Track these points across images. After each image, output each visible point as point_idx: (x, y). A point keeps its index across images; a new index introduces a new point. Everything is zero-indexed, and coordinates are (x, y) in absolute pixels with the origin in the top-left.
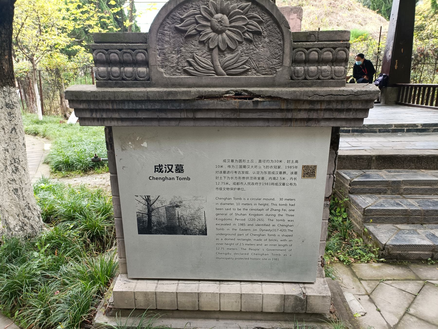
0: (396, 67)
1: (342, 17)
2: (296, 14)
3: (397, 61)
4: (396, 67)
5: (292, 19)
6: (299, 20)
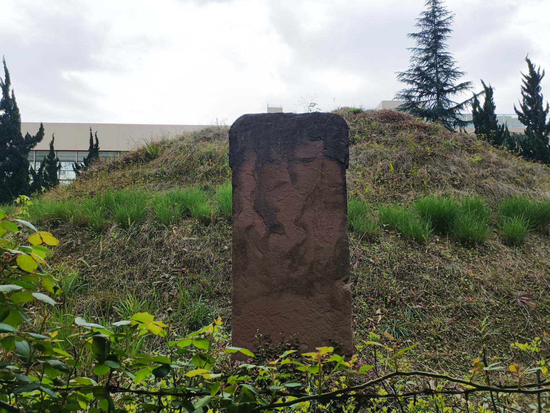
1: (460, 164)
5: (304, 160)
6: (332, 167)
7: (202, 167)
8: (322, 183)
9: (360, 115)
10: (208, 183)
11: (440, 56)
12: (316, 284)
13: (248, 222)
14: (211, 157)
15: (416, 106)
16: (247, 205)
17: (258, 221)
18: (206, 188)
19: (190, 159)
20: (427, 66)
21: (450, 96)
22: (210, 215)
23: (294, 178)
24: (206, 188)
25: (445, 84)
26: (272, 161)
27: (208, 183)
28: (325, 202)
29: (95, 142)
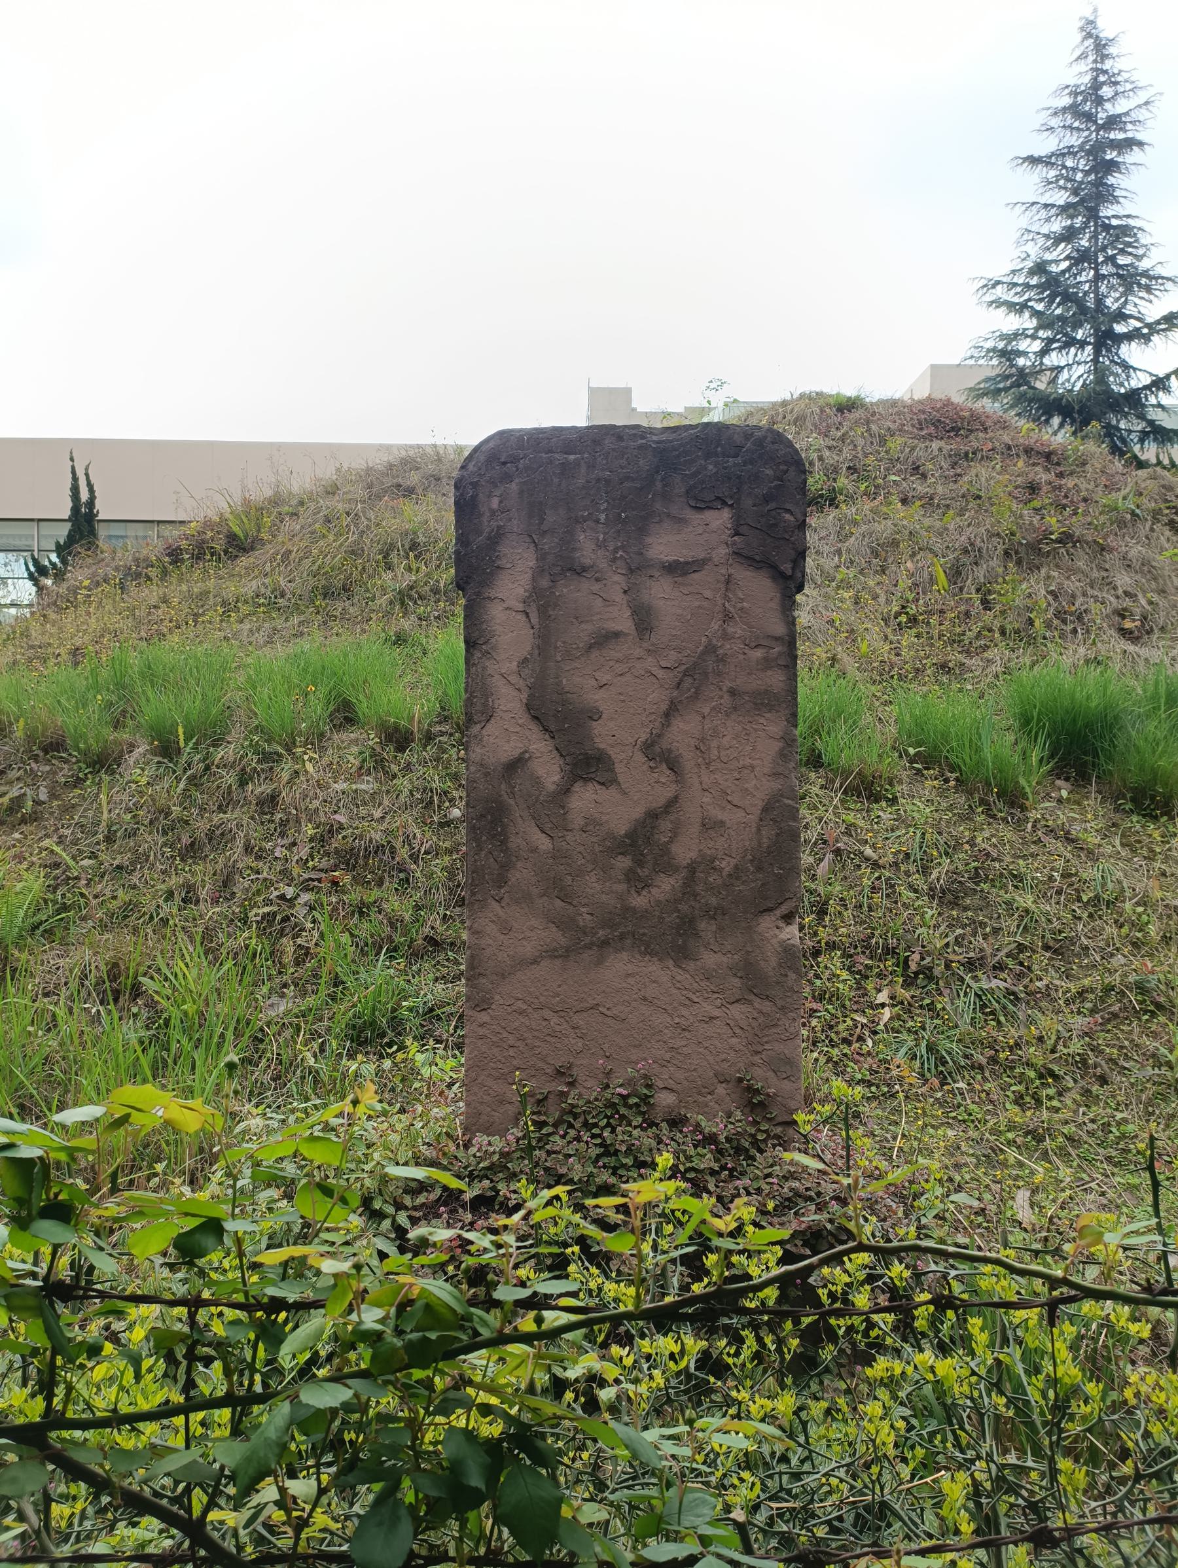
2: (721, 519)
5: (676, 569)
6: (757, 588)
7: (390, 574)
8: (726, 636)
9: (857, 414)
10: (406, 624)
11: (1107, 228)
12: (702, 925)
13: (508, 750)
14: (414, 546)
15: (1027, 383)
16: (509, 700)
17: (540, 746)
18: (400, 640)
19: (356, 552)
20: (1068, 258)
21: (1131, 352)
22: (411, 719)
23: (644, 620)
24: (400, 640)
25: (1121, 316)
26: (580, 571)
27: (406, 624)
28: (733, 692)
29: (84, 496)
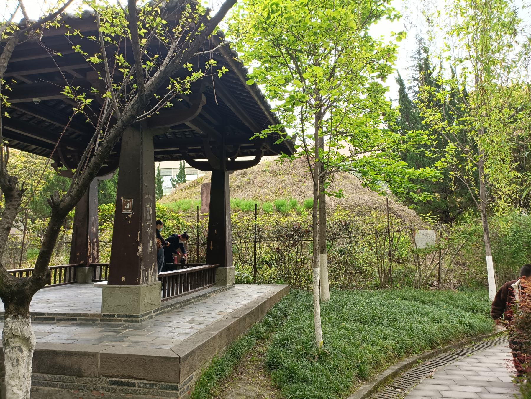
0: (211, 248)
3: (211, 242)
4: (211, 248)
16: (204, 204)
